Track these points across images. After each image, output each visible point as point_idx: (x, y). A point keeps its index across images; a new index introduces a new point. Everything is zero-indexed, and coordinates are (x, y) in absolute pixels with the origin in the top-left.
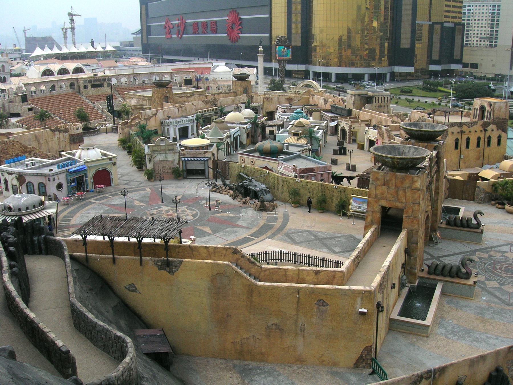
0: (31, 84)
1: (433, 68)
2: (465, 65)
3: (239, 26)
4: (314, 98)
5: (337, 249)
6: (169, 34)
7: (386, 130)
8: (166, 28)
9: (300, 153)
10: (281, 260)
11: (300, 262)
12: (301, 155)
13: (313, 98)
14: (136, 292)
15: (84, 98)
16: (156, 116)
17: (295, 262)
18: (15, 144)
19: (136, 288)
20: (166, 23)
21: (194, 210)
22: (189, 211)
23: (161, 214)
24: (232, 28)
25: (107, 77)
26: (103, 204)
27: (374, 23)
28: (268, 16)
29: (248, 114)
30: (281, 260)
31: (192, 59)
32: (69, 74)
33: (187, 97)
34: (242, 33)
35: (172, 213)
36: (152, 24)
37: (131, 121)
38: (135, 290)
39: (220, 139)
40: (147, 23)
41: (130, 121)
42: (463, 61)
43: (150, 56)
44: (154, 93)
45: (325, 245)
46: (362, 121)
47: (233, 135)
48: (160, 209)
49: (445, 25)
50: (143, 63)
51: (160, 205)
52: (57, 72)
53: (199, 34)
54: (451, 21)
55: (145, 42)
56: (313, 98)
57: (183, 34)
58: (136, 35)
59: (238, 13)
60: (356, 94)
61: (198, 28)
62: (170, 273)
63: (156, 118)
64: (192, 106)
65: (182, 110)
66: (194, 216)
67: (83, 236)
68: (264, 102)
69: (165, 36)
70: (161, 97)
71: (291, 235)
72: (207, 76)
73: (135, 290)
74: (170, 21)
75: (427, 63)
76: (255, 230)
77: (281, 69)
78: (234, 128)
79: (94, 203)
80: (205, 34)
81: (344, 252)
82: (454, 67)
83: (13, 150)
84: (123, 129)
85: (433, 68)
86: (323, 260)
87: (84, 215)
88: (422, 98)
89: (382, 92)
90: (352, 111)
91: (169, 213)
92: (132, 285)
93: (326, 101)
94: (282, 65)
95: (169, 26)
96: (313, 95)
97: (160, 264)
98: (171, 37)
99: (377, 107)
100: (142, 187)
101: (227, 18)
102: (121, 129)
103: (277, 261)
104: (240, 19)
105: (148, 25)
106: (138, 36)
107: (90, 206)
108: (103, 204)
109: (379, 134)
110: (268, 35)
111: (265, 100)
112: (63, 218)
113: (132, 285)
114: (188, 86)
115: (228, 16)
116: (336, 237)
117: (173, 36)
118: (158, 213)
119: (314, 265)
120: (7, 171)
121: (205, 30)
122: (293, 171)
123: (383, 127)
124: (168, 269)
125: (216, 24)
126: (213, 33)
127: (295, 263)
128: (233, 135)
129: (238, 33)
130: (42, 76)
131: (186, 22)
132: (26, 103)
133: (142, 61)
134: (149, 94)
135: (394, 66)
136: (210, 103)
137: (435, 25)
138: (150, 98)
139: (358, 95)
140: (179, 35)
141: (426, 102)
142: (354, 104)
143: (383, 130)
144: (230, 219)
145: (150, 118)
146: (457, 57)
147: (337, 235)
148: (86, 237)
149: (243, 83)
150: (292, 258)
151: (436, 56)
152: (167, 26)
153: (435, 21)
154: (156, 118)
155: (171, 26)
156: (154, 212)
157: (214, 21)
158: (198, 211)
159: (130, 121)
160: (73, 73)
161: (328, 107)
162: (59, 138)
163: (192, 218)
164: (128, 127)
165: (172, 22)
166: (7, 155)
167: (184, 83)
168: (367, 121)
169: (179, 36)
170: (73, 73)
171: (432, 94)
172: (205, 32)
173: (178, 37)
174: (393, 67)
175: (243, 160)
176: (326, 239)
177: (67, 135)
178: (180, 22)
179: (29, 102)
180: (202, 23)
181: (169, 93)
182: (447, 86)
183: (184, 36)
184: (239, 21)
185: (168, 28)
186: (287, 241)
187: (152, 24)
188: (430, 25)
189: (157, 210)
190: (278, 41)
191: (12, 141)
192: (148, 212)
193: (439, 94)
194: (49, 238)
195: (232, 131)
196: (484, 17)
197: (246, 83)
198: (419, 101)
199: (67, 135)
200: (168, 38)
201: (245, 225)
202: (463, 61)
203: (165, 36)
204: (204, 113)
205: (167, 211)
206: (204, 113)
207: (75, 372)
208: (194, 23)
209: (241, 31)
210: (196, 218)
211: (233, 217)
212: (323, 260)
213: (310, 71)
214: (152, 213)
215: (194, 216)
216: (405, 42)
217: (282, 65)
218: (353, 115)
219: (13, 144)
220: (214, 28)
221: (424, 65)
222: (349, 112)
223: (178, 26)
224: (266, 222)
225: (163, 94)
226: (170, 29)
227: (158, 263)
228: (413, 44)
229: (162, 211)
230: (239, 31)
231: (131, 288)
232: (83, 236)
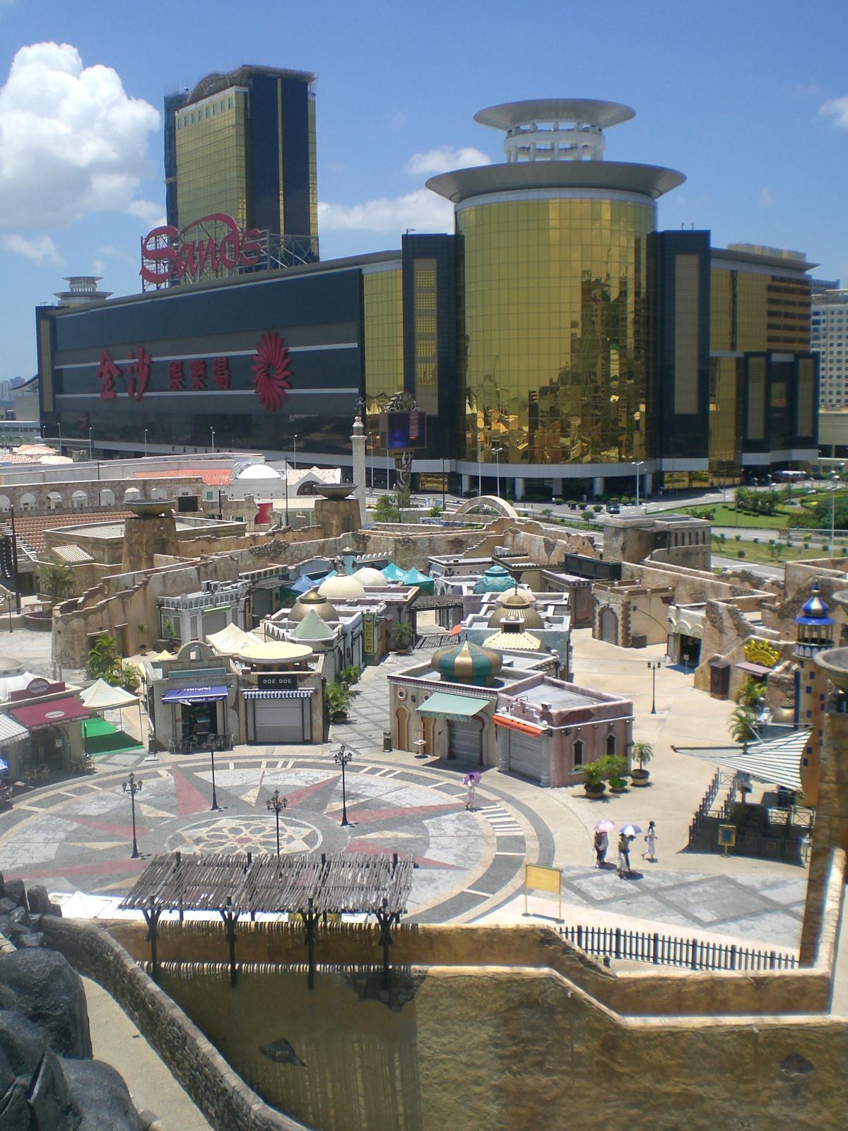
1: (751, 459)
2: (825, 451)
3: (285, 369)
4: (517, 540)
5: (706, 916)
7: (729, 611)
8: (101, 374)
9: (541, 673)
10: (617, 952)
11: (598, 950)
12: (546, 677)
13: (514, 538)
14: (292, 1062)
16: (145, 589)
17: (655, 958)
19: (292, 1051)
20: (103, 364)
21: (305, 826)
22: (293, 828)
23: (221, 837)
24: (268, 376)
26: (57, 815)
28: (355, 345)
29: (372, 580)
30: (617, 952)
31: (167, 448)
33: (209, 540)
34: (291, 388)
35: (249, 835)
37: (85, 600)
38: (290, 1058)
39: (324, 642)
40: (53, 362)
41: (81, 600)
42: (821, 441)
43: (63, 442)
44: (128, 530)
45: (672, 907)
46: (654, 591)
47: (352, 633)
48: (214, 826)
49: (776, 358)
50: (47, 456)
51: (212, 816)
53: (184, 389)
54: (783, 348)
55: (49, 408)
56: (514, 538)
59: (282, 340)
60: (628, 526)
61: (183, 376)
62: (389, 1004)
63: (145, 594)
64: (231, 562)
65: (206, 573)
66: (310, 840)
67: (149, 912)
68: (396, 550)
70: (148, 541)
71: (575, 883)
72: (184, 491)
73: (290, 1058)
74: (112, 360)
75: (736, 450)
76: (478, 872)
77: (401, 471)
78: (350, 614)
79: (31, 813)
80: (200, 389)
81: (724, 920)
82: (797, 454)
84: (66, 621)
85: (751, 459)
86: (694, 944)
87: (16, 845)
88: (745, 531)
89: (687, 519)
90: (623, 568)
91: (242, 835)
92: (283, 1043)
93: (549, 547)
94: (404, 461)
95: (109, 372)
96: (515, 532)
97: (364, 982)
98: (116, 397)
99: (680, 557)
100: (147, 767)
101: (255, 352)
102: (60, 623)
103: (608, 954)
104: (287, 354)
105: (57, 367)
107: (25, 822)
108: (57, 815)
109: (711, 621)
110: (356, 390)
111: (399, 545)
112: (486, 898)
113: (283, 1043)
114: (188, 513)
115: (258, 346)
116: (690, 884)
117: (119, 395)
118: (211, 837)
119: (707, 965)
121: (202, 381)
122: (542, 719)
123: (721, 603)
124: (385, 995)
125: (227, 367)
127: (655, 962)
128: (352, 633)
129: (283, 388)
133: (49, 455)
134: (115, 532)
135: (662, 457)
136: (268, 554)
137: (752, 360)
138: (114, 544)
139: (633, 528)
141: (756, 541)
142: (623, 549)
143: (721, 611)
144: (405, 848)
145: (132, 593)
146: (803, 430)
147: (691, 879)
148: (155, 917)
149: (342, 506)
150: (648, 948)
151: (756, 430)
152: (105, 371)
153: (749, 351)
154: (145, 594)
155: (116, 373)
156: (203, 832)
157: (221, 358)
158: (314, 828)
159: (81, 600)
161: (557, 557)
163: (306, 847)
164: (78, 615)
165: (117, 362)
167: (177, 507)
168: (666, 590)
169: (136, 394)
171: (762, 520)
172: (202, 386)
173: (132, 396)
174: (658, 459)
175: (401, 694)
176: (666, 889)
178: (137, 360)
180: (216, 364)
181: (167, 530)
182: (792, 500)
184: (285, 358)
185: (108, 376)
186: (572, 900)
188: (738, 360)
189: (208, 829)
190: (392, 406)
192: (185, 834)
193: (782, 521)
194: (51, 922)
195: (348, 621)
196: (835, 344)
197: (347, 505)
198: (738, 538)
200: (106, 400)
201: (450, 860)
202: (821, 441)
204: (256, 579)
205: (234, 831)
206: (256, 579)
208: (173, 363)
209: (289, 383)
210: (316, 847)
211: (410, 841)
212: (733, 950)
213: (461, 475)
214: (197, 836)
215: (310, 840)
216: (684, 401)
217: (404, 461)
218: (625, 576)
220: (225, 373)
221: (726, 455)
222: (615, 572)
223: (133, 371)
224: (498, 851)
225: (154, 534)
226: (112, 378)
227: (359, 981)
228: (704, 405)
229: (220, 829)
230: (282, 383)
231: (278, 1053)
232: (149, 912)
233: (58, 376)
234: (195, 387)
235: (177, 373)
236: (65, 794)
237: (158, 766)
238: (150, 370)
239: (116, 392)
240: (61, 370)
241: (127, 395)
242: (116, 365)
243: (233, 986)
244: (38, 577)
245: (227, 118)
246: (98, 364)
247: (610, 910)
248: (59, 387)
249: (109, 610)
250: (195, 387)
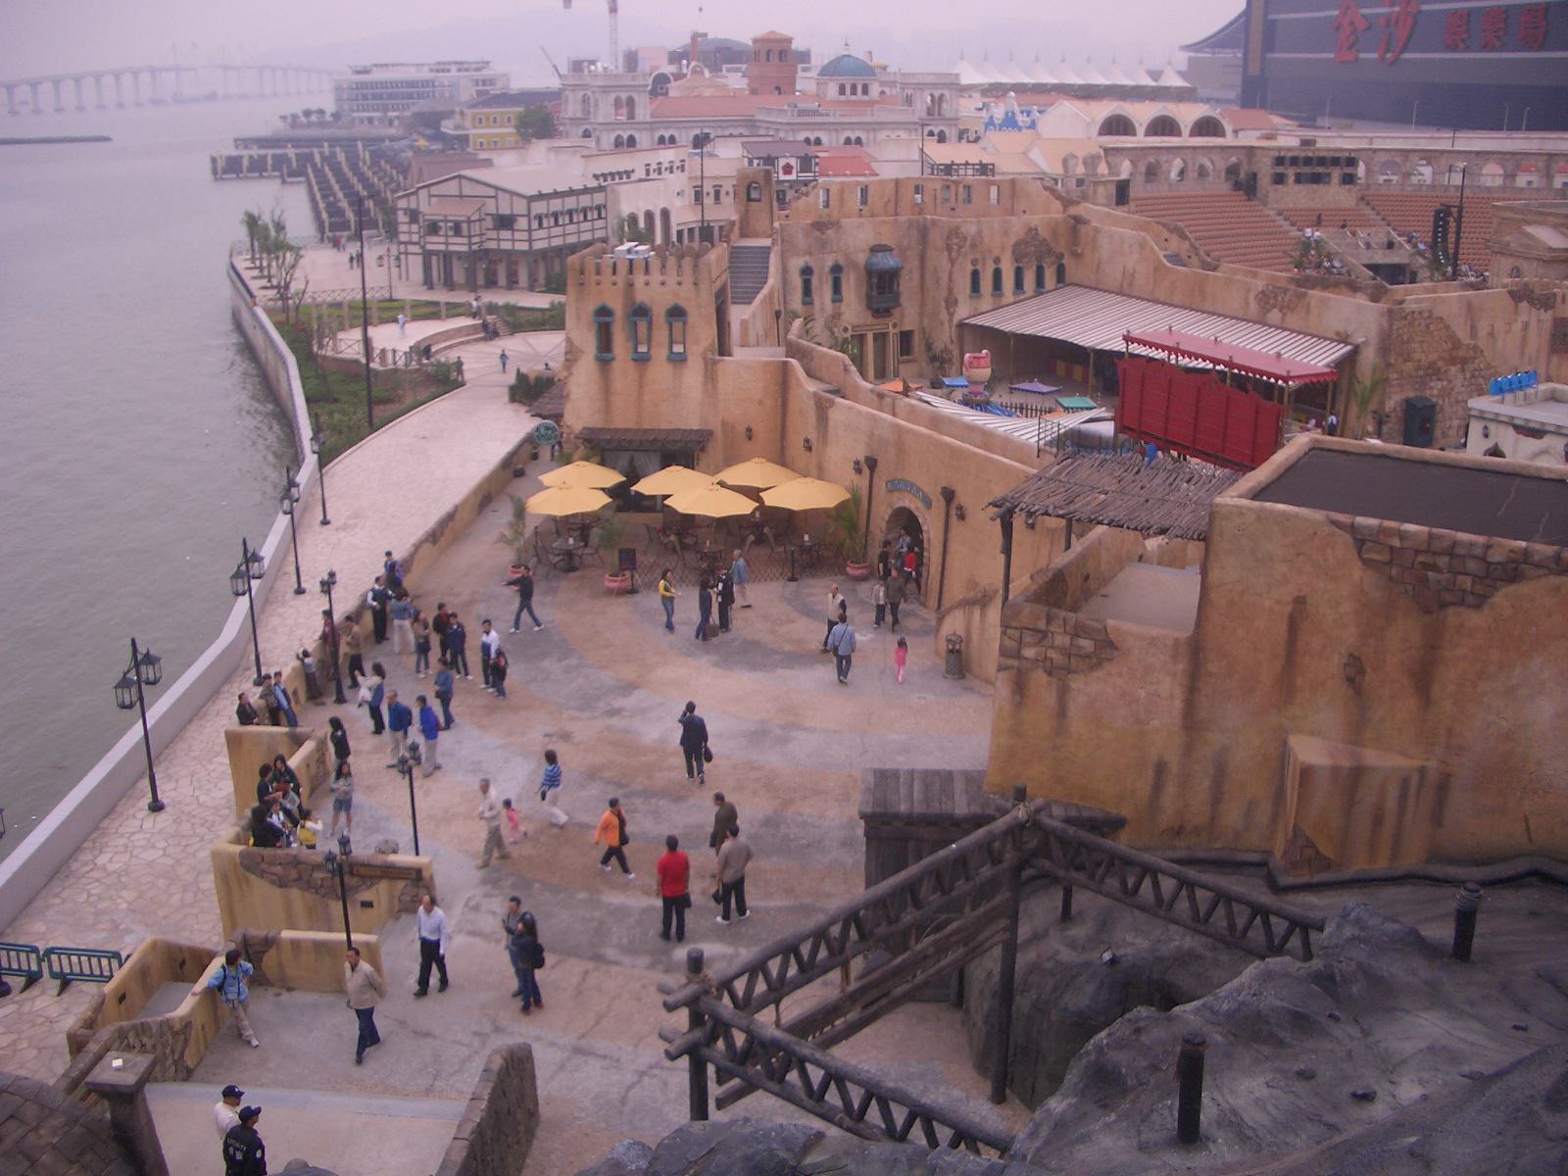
0: (1123, 149)
6: (1350, 48)
15: (1272, 213)
18: (1432, 327)
20: (1344, 14)
25: (1346, 154)
27: (887, 172)
32: (1134, 135)
36: (1282, 16)
52: (1145, 126)
53: (1467, 49)
55: (1254, 70)
57: (1404, 49)
58: (1197, 51)
69: (1332, 55)
80: (1493, 49)
83: (1425, 346)
98: (1357, 60)
105: (1270, 17)
106: (1200, 55)
117: (1362, 56)
120: (1518, 422)
126: (1531, 49)
130: (1100, 134)
131: (1420, 12)
132: (1126, 208)
140: (1387, 50)
160: (1193, 134)
162: (1526, 326)
166: (1406, 361)
169: (1389, 55)
170: (1193, 134)
173: (1382, 58)
177: (1547, 316)
178: (1397, 9)
179: (1132, 205)
183: (1406, 56)
187: (1282, 16)
191: (1426, 314)
199: (1547, 316)
203: (1332, 55)
207: (240, 705)
219: (1427, 326)
233: (1270, 28)
234: (1485, 47)
235: (1460, 26)
236: (824, 394)
237: (650, 123)
238: (1415, 23)
239: (1358, 51)
240: (1275, 21)
241: (1375, 56)
242: (1363, 15)
243: (526, 1009)
244: (1279, 355)
245: (1042, 436)
246: (1336, 13)
247: (286, 528)
248: (1269, 45)
249: (894, 1100)
250: (1485, 47)
